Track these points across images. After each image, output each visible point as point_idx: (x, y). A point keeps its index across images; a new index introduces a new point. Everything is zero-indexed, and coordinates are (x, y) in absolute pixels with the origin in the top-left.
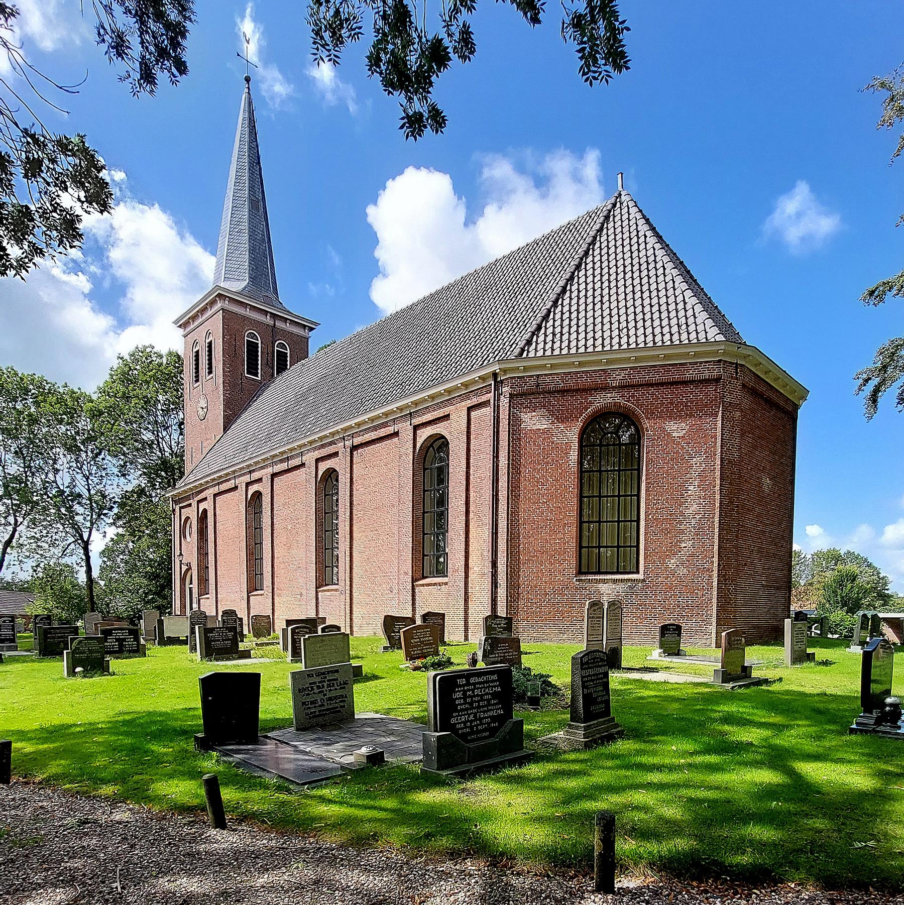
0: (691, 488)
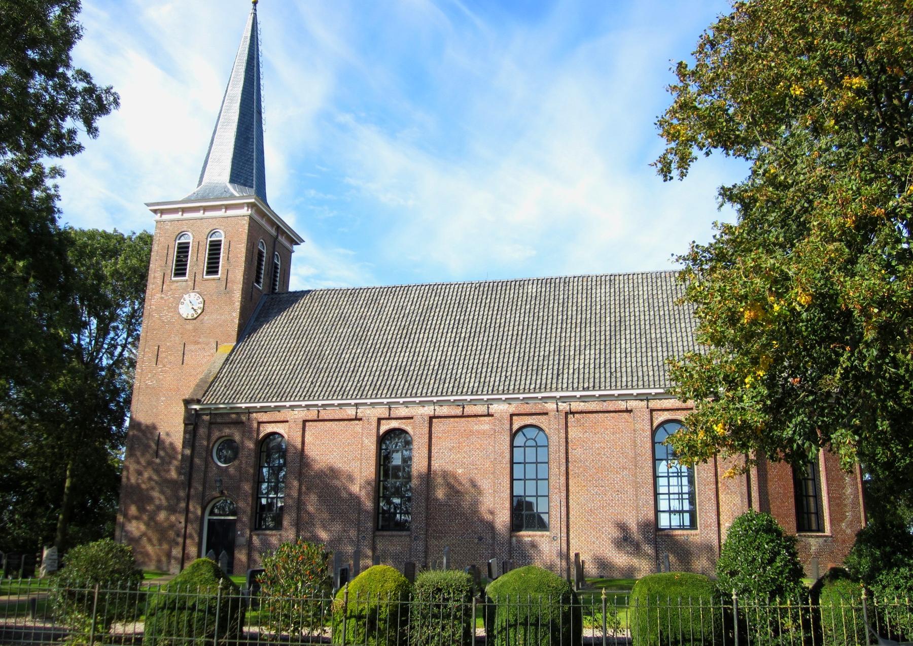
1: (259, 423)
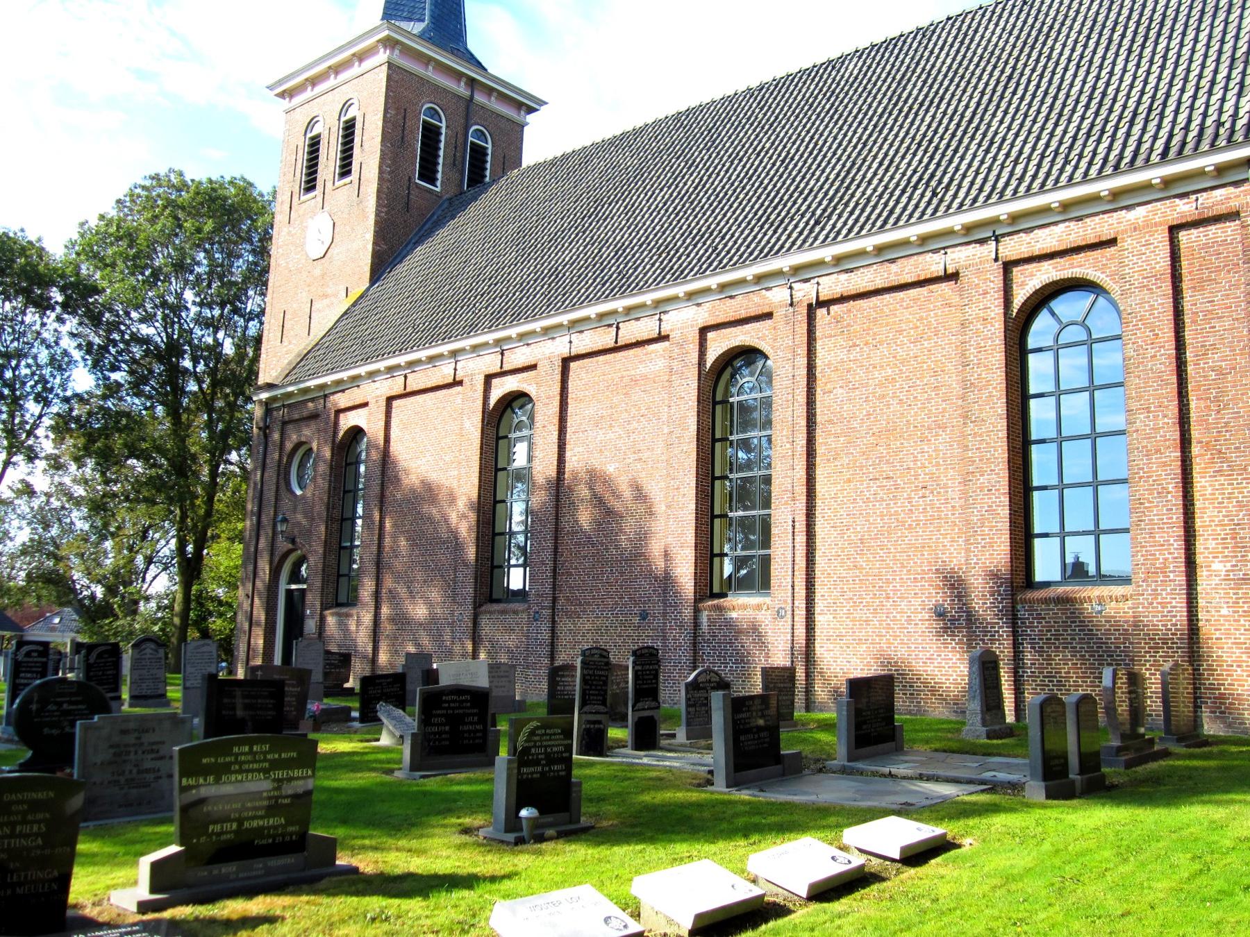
1: (339, 412)
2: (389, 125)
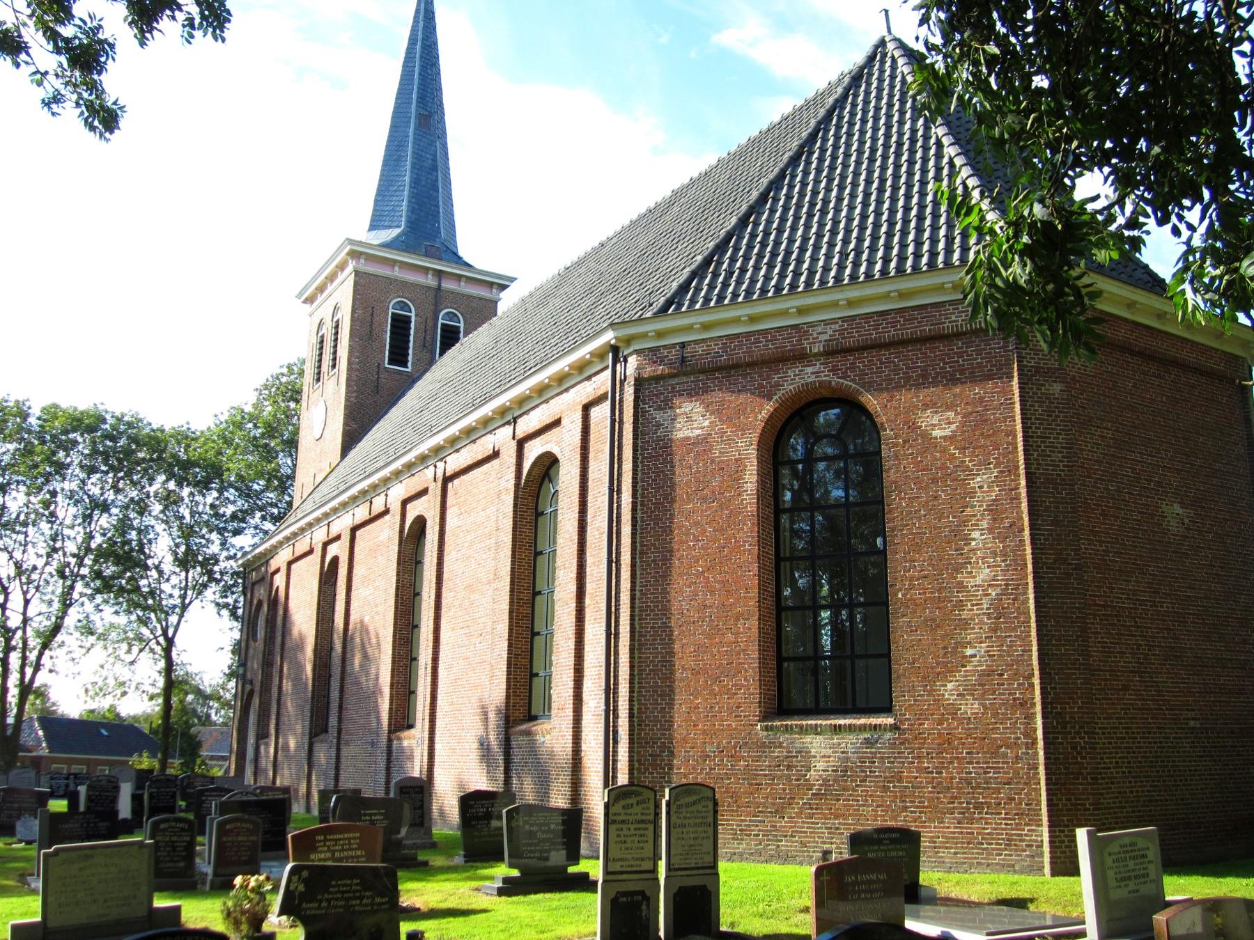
0: (976, 534)
2: (358, 323)
